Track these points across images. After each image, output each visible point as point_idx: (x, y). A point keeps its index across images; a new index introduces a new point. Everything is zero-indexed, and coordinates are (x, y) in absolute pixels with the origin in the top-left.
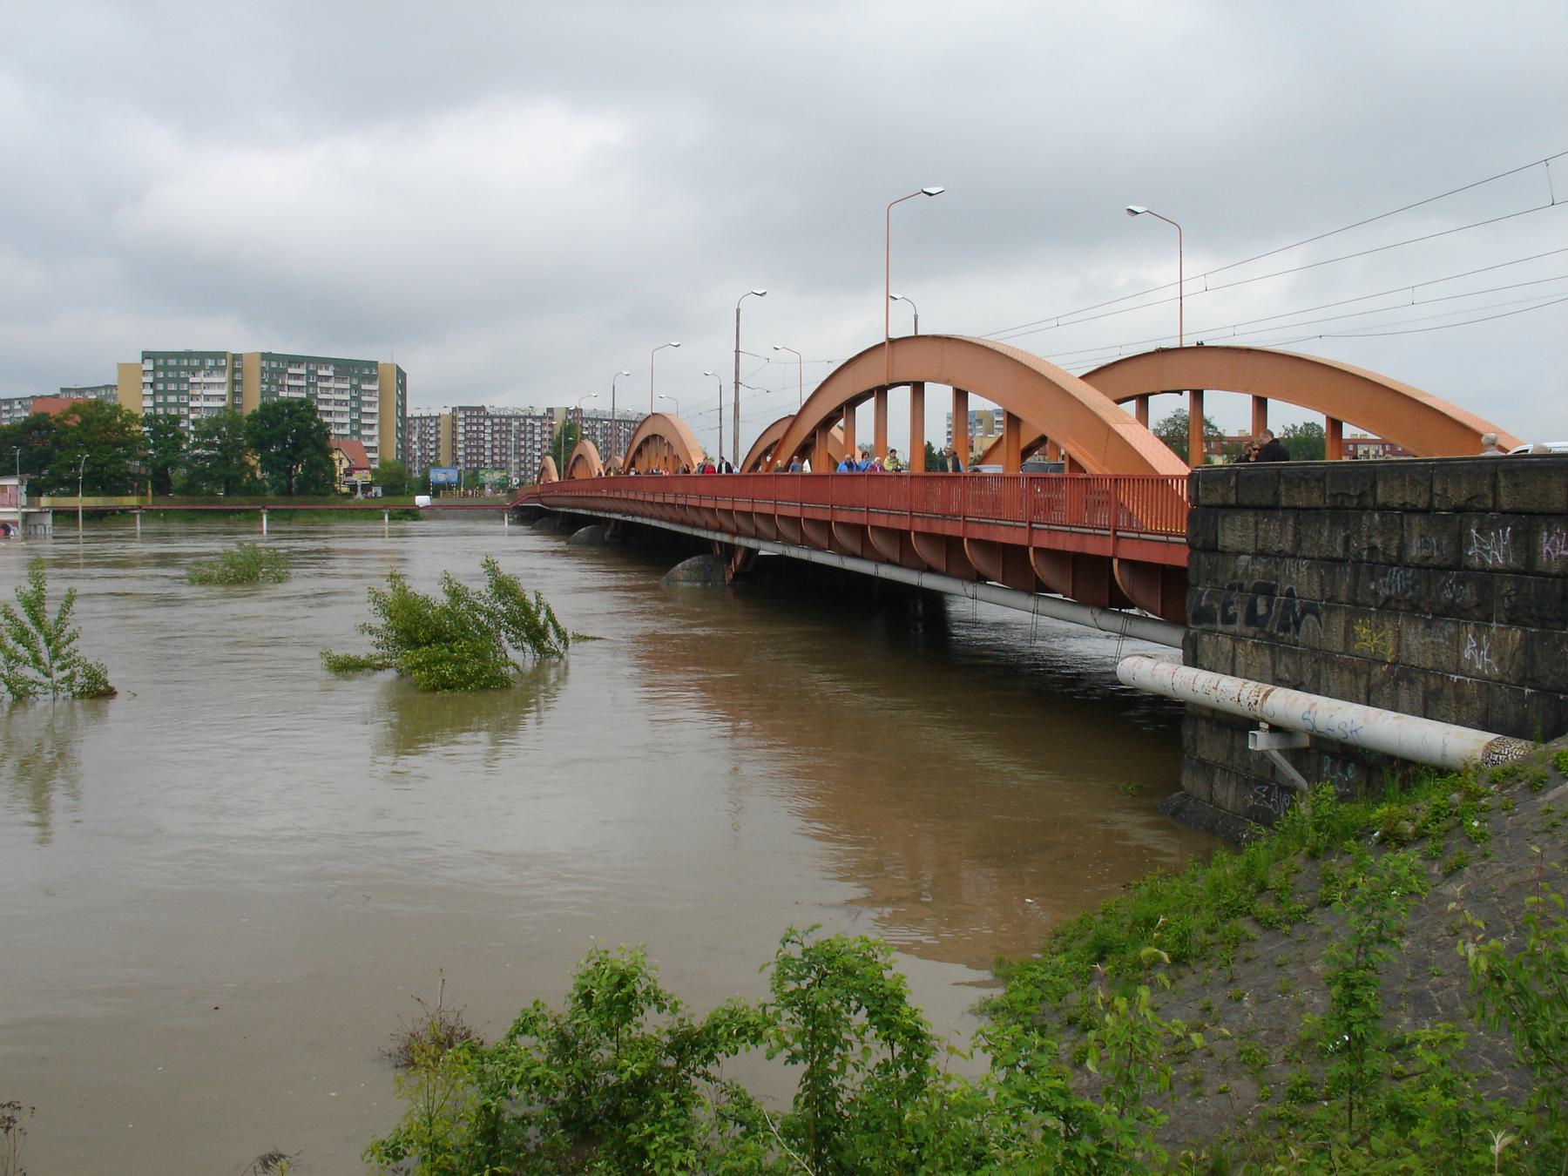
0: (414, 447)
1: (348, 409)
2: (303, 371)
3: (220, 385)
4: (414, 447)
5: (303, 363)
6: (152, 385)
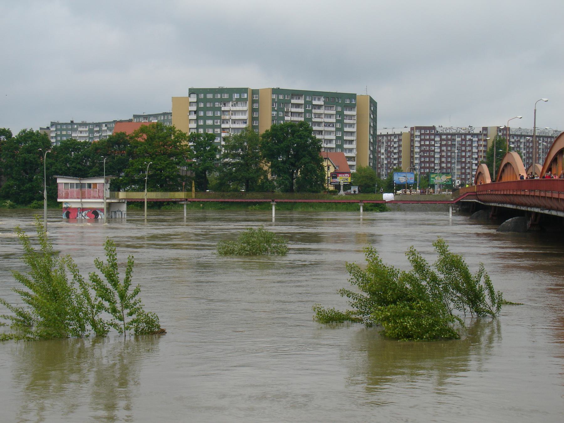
0: (382, 157)
1: (333, 129)
2: (301, 101)
3: (243, 112)
4: (382, 157)
5: (302, 96)
6: (195, 112)
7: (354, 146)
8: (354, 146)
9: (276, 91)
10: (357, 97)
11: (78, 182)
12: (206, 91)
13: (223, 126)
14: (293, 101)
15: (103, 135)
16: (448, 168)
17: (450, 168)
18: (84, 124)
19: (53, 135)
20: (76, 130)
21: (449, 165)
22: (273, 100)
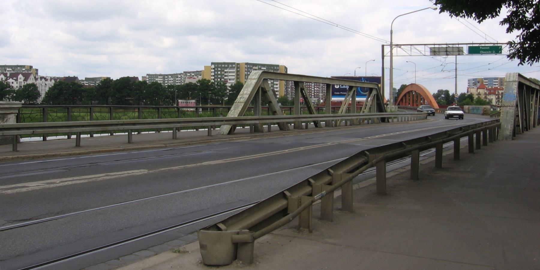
4: (289, 90)
7: (278, 86)
8: (278, 86)
9: (247, 64)
10: (279, 67)
11: (186, 101)
12: (218, 64)
13: (225, 74)
14: (254, 68)
15: (169, 80)
16: (317, 95)
17: (318, 95)
18: (160, 75)
19: (148, 79)
20: (157, 78)
21: (318, 94)
22: (246, 67)
